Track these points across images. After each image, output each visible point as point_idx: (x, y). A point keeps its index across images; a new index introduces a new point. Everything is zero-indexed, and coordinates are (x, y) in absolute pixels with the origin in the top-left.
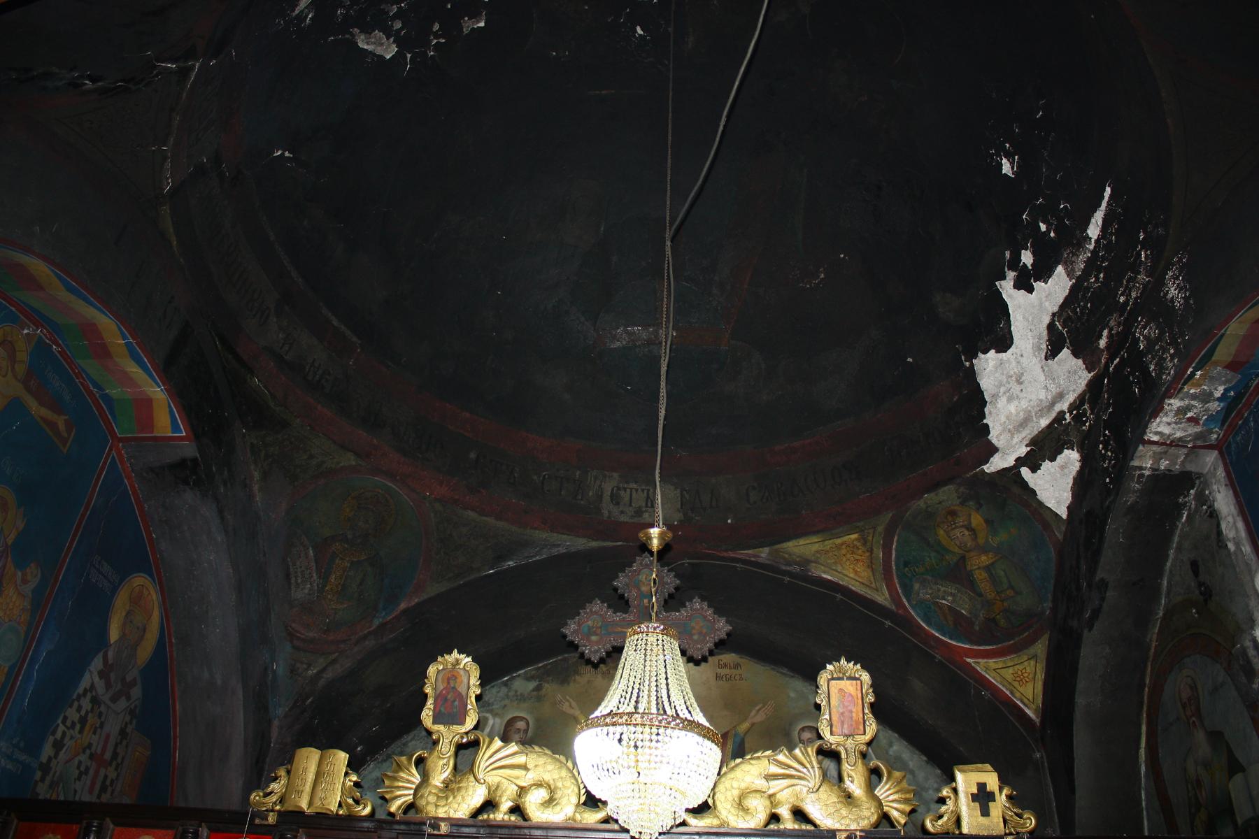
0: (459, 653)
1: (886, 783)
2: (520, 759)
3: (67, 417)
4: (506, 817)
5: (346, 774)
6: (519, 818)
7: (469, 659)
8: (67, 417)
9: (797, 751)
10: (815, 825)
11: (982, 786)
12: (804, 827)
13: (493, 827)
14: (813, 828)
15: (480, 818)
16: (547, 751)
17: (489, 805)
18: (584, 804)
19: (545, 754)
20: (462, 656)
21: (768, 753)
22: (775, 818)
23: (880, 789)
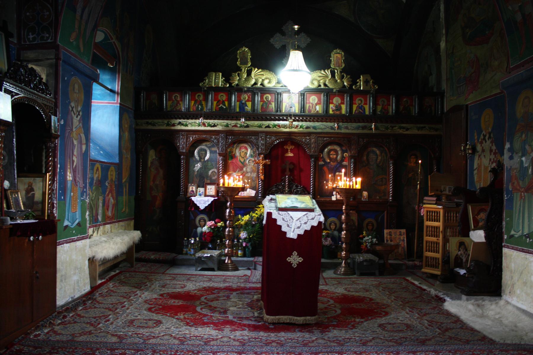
2: (262, 73)
11: (367, 79)
17: (255, 84)
21: (319, 71)
22: (320, 86)
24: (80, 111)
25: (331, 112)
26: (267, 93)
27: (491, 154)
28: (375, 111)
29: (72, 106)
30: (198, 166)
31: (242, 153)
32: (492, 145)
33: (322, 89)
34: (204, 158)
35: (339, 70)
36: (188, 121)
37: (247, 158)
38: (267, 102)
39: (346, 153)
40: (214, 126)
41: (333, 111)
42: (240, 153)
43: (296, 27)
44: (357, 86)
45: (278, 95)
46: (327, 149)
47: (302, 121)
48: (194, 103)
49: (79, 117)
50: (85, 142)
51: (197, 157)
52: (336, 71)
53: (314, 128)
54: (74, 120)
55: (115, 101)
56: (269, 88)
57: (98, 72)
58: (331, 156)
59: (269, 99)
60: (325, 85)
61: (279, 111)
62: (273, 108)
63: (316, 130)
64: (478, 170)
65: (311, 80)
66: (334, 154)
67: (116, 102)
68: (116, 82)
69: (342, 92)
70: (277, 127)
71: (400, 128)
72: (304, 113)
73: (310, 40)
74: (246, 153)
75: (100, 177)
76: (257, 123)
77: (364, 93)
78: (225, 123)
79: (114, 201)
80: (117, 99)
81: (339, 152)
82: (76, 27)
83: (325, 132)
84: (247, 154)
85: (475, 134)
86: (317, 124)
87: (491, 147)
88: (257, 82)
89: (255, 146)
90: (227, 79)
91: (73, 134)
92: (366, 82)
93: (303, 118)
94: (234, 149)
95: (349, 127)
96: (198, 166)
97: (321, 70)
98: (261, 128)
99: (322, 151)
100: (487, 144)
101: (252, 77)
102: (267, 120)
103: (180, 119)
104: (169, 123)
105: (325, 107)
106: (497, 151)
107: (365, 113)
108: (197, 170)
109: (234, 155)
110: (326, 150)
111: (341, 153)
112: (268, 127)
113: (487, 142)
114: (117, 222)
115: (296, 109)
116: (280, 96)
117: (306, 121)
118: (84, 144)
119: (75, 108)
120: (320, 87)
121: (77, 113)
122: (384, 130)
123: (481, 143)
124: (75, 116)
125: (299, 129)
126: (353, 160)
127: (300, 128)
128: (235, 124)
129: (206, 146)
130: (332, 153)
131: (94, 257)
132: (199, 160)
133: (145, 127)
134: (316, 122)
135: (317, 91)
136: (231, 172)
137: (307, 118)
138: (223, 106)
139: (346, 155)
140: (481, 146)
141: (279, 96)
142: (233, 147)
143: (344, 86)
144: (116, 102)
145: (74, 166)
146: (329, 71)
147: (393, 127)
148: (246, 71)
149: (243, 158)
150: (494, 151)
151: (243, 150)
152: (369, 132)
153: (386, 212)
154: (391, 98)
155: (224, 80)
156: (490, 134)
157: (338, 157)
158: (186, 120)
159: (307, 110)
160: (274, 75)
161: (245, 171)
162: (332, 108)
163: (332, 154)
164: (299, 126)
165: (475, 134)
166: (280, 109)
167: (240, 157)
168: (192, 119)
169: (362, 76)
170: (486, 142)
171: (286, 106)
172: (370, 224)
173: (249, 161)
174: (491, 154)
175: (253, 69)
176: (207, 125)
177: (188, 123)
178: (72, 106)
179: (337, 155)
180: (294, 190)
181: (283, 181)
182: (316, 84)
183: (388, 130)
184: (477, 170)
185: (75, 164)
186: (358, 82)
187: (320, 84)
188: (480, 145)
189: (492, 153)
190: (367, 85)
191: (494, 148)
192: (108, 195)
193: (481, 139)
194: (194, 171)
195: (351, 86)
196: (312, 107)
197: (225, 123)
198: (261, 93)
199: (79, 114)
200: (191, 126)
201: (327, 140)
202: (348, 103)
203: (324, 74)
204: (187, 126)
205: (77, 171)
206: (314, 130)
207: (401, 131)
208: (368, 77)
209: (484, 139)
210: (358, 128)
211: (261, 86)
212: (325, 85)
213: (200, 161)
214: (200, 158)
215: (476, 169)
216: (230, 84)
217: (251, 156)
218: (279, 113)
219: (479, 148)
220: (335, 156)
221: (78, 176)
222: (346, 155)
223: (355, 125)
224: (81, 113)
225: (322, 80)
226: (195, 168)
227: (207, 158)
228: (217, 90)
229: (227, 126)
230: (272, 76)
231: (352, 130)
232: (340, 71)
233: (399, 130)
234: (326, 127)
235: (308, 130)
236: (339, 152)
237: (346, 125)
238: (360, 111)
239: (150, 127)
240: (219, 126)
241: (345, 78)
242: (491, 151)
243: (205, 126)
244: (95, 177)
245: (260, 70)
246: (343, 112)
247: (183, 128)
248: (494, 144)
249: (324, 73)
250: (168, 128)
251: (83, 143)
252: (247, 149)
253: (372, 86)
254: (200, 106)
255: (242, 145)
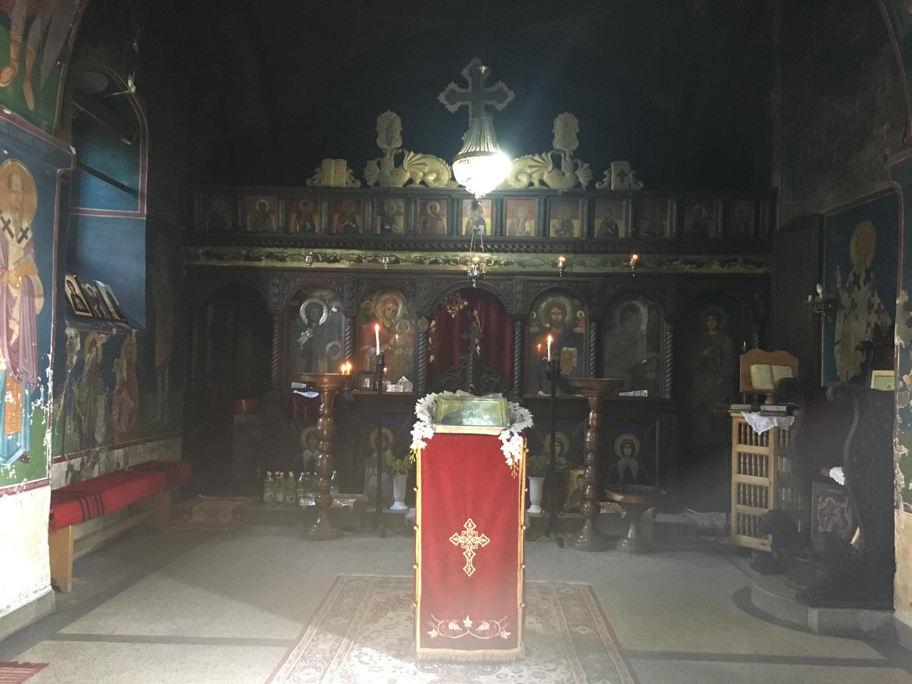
0: (391, 111)
1: (580, 170)
2: (422, 161)
3: (907, 455)
4: (419, 186)
5: (347, 169)
6: (424, 186)
7: (395, 114)
8: (907, 455)
9: (544, 155)
10: (549, 187)
11: (622, 170)
12: (544, 187)
13: (411, 189)
14: (547, 188)
15: (408, 186)
16: (429, 155)
17: (411, 181)
18: (451, 179)
19: (430, 157)
20: (392, 113)
21: (531, 156)
22: (532, 184)
23: (521, 545)
24: (27, 229)
25: (552, 234)
26: (432, 200)
27: (869, 313)
28: (635, 234)
29: (6, 220)
30: (306, 335)
31: (387, 310)
32: (873, 295)
33: (536, 190)
34: (318, 321)
35: (568, 154)
36: (286, 251)
37: (396, 320)
38: (433, 215)
39: (581, 310)
40: (336, 260)
41: (556, 232)
42: (384, 310)
43: (484, 68)
44: (603, 183)
45: (453, 202)
46: (545, 303)
47: (498, 251)
48: (297, 218)
49: (25, 242)
50: (42, 292)
51: (306, 320)
52: (562, 155)
53: (521, 264)
54: (10, 247)
55: (138, 210)
56: (436, 189)
57: (71, 152)
58: (553, 317)
59: (438, 210)
60: (542, 182)
61: (455, 234)
62: (444, 227)
63: (525, 268)
64: (842, 345)
65: (516, 174)
66: (558, 314)
67: (139, 212)
68: (139, 173)
69: (573, 194)
70: (451, 262)
71: (686, 262)
72: (502, 235)
73: (514, 96)
74: (395, 312)
75: (100, 357)
76: (415, 255)
77: (618, 195)
78: (355, 256)
79: (134, 401)
80: (142, 209)
81: (569, 309)
82: (13, 56)
83: (541, 272)
84: (397, 312)
85: (838, 273)
86: (526, 257)
87: (870, 299)
88: (414, 179)
89: (409, 295)
90: (358, 172)
91: (8, 276)
92: (622, 175)
93: (499, 246)
94: (373, 305)
95: (588, 262)
96: (306, 335)
97: (534, 155)
98: (421, 265)
99: (534, 306)
100: (863, 293)
101: (404, 169)
102: (432, 249)
103: (270, 246)
104: (251, 254)
105: (541, 224)
106: (882, 307)
107: (617, 234)
108: (303, 343)
109: (374, 314)
110: (544, 305)
111: (572, 310)
112: (436, 262)
113: (861, 290)
114: (141, 444)
115: (487, 227)
116: (458, 205)
117: (505, 251)
118: (39, 296)
119: (15, 224)
120: (531, 188)
121: (21, 234)
122: (653, 266)
123: (850, 291)
124: (15, 239)
125: (493, 267)
126: (594, 324)
127: (494, 264)
128: (373, 258)
129: (322, 298)
130: (555, 310)
131: (55, 534)
132: (307, 323)
133: (203, 262)
134: (525, 254)
135: (527, 193)
136: (367, 347)
137: (521, 246)
138: (351, 224)
139: (581, 314)
140: (849, 296)
141: (456, 204)
142: (371, 300)
143: (578, 185)
144: (139, 212)
145: (12, 342)
146: (549, 155)
147: (671, 261)
148: (393, 157)
149: (390, 320)
150: (876, 307)
151: (390, 305)
152: (626, 270)
153: (658, 422)
154: (669, 204)
155: (352, 174)
156: (868, 273)
157: (567, 318)
158: (281, 250)
159: (507, 231)
160: (445, 165)
161: (393, 344)
162: (554, 226)
163: (554, 313)
164: (493, 262)
165: (838, 273)
166: (457, 229)
167: (384, 319)
168: (293, 247)
169: (614, 164)
170: (859, 288)
171: (468, 223)
172: (627, 445)
173: (400, 326)
174: (869, 313)
175: (406, 152)
176: (320, 259)
177: (285, 255)
178: (6, 220)
179: (564, 313)
180: (484, 379)
181: (463, 363)
182: (524, 180)
183: (661, 267)
184: (840, 344)
185: (15, 337)
186: (605, 176)
187: (532, 181)
188: (848, 294)
189: (873, 311)
190: (622, 181)
191: (877, 300)
192: (119, 392)
193: (850, 283)
194: (298, 345)
195: (591, 185)
196: (518, 225)
197: (355, 256)
198: (421, 199)
199: (24, 236)
200: (291, 261)
201: (545, 286)
202: (585, 215)
203: (538, 162)
204: (285, 261)
205: (21, 351)
206: (520, 268)
207: (687, 268)
208: (625, 165)
209: (856, 282)
210: (604, 264)
211: (422, 186)
212: (542, 182)
213: (309, 326)
214: (310, 321)
215: (838, 343)
216: (364, 182)
217: (404, 316)
218: (455, 237)
219: (845, 300)
220: (560, 317)
221: (24, 361)
222: (581, 314)
223: (597, 259)
224: (30, 234)
225: (535, 172)
226: (301, 339)
227: (323, 320)
228: (336, 194)
229: (359, 260)
230: (442, 166)
231: (593, 267)
232: (570, 155)
233: (683, 266)
234: (543, 263)
235: (510, 269)
236: (569, 309)
237: (580, 259)
238: (608, 231)
239: (213, 262)
240: (345, 261)
241: (579, 168)
242: (870, 306)
243: (318, 261)
244: (88, 357)
245: (419, 156)
246: (576, 233)
247: (279, 264)
248: (876, 293)
249: (540, 160)
250: (248, 263)
251: (36, 294)
252: (397, 305)
253: (632, 182)
254: (308, 224)
255: (386, 297)
